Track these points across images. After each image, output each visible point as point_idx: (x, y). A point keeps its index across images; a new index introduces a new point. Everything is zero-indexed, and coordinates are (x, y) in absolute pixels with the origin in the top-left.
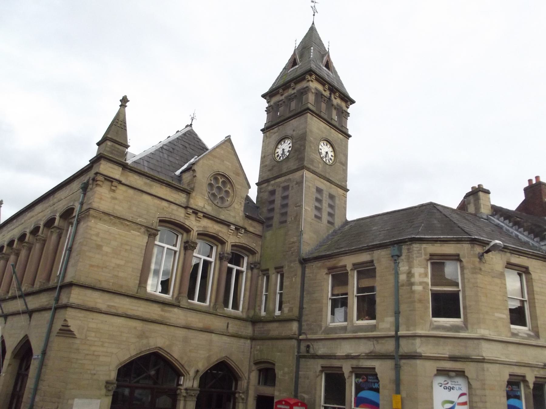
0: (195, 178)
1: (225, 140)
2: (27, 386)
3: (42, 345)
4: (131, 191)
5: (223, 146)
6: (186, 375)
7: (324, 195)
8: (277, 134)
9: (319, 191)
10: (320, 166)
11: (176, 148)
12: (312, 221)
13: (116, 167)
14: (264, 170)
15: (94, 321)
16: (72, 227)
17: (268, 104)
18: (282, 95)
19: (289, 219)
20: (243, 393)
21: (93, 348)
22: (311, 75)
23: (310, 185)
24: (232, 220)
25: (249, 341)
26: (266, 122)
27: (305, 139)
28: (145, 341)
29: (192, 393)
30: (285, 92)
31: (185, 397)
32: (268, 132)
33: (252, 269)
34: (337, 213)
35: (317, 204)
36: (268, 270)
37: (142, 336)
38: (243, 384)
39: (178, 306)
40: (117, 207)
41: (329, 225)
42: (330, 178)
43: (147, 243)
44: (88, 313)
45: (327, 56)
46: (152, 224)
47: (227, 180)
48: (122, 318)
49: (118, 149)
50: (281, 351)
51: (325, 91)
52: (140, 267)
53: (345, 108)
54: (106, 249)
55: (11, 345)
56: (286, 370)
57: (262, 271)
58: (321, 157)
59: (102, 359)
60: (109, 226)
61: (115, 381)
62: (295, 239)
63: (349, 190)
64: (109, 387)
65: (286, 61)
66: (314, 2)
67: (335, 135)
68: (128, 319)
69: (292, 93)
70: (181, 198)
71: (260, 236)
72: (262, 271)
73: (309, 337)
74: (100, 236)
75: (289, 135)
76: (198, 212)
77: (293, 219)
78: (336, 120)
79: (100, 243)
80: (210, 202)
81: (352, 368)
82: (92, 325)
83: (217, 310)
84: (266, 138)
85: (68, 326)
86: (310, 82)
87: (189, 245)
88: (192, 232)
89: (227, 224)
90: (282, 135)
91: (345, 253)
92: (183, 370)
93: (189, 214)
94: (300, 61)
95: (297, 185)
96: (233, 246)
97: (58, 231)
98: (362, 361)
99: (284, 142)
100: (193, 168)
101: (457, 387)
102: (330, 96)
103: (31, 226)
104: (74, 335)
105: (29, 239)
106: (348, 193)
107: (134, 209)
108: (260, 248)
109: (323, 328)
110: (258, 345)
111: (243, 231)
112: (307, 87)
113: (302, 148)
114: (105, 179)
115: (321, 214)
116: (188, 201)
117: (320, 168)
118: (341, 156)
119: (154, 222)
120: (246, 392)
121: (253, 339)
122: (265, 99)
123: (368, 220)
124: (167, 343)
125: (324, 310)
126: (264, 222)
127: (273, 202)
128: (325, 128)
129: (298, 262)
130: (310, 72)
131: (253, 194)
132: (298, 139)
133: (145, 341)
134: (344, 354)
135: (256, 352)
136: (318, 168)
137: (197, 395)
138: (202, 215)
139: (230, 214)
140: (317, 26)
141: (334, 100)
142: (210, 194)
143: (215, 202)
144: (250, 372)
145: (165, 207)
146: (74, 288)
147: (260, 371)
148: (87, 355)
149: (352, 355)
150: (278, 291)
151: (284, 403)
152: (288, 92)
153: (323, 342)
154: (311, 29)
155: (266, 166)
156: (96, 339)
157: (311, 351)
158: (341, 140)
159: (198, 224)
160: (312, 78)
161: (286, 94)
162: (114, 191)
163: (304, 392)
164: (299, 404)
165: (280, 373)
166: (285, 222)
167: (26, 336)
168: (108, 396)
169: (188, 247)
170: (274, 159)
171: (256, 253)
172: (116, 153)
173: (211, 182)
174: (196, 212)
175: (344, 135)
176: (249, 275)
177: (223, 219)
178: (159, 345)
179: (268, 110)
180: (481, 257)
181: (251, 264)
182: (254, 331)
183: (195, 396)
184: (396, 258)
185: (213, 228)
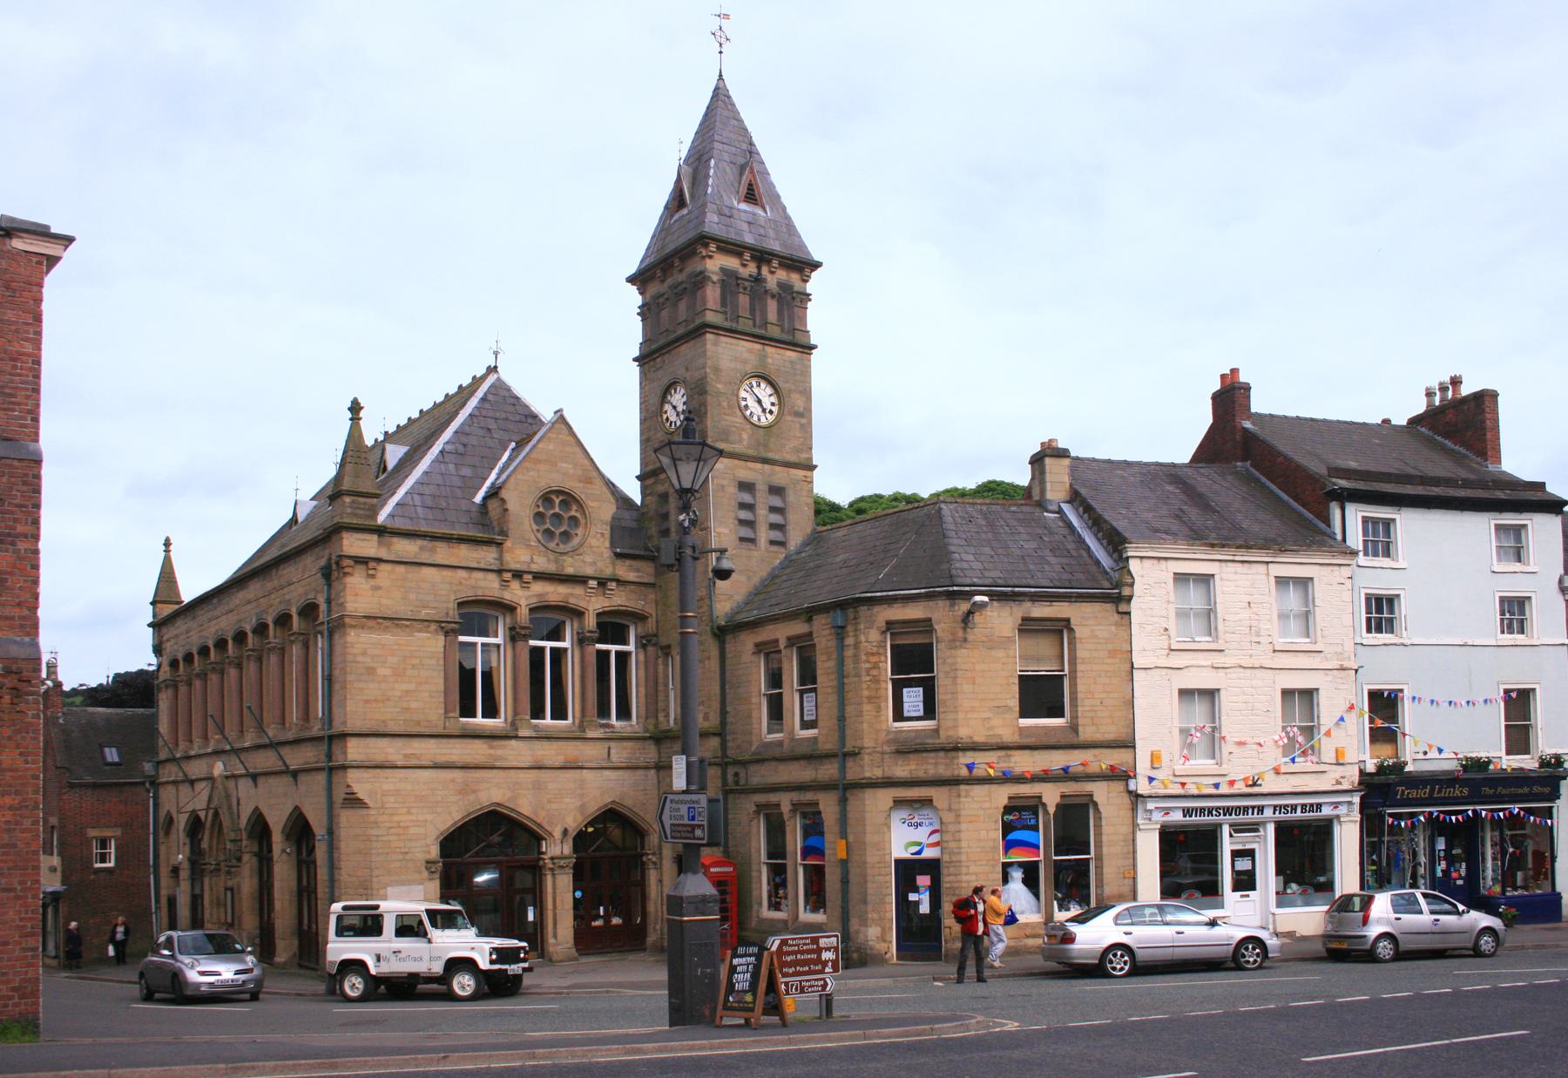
3: (325, 819)
4: (401, 569)
9: (746, 487)
10: (745, 436)
16: (322, 637)
20: (654, 854)
21: (396, 818)
27: (706, 392)
28: (472, 797)
29: (562, 862)
31: (552, 869)
33: (644, 646)
35: (744, 515)
36: (669, 647)
37: (463, 792)
39: (516, 737)
40: (384, 601)
43: (445, 646)
44: (378, 771)
46: (447, 614)
47: (568, 499)
51: (744, 266)
52: (442, 688)
53: (797, 285)
54: (382, 671)
55: (277, 821)
57: (662, 648)
58: (745, 417)
61: (438, 859)
67: (778, 357)
70: (487, 556)
71: (652, 585)
72: (662, 648)
79: (372, 665)
80: (544, 549)
81: (793, 805)
82: (385, 787)
87: (517, 633)
88: (518, 610)
89: (580, 580)
90: (665, 381)
96: (598, 615)
99: (675, 392)
101: (927, 821)
102: (759, 273)
104: (365, 804)
107: (412, 596)
108: (653, 605)
113: (703, 408)
116: (500, 559)
117: (743, 443)
124: (509, 794)
125: (755, 714)
128: (750, 351)
136: (741, 441)
137: (571, 865)
138: (530, 577)
139: (583, 561)
141: (769, 278)
146: (348, 739)
148: (390, 828)
159: (527, 593)
161: (669, 281)
162: (373, 576)
167: (297, 808)
171: (647, 618)
174: (518, 575)
176: (642, 657)
179: (645, 312)
180: (966, 619)
181: (643, 637)
184: (840, 632)
185: (556, 593)
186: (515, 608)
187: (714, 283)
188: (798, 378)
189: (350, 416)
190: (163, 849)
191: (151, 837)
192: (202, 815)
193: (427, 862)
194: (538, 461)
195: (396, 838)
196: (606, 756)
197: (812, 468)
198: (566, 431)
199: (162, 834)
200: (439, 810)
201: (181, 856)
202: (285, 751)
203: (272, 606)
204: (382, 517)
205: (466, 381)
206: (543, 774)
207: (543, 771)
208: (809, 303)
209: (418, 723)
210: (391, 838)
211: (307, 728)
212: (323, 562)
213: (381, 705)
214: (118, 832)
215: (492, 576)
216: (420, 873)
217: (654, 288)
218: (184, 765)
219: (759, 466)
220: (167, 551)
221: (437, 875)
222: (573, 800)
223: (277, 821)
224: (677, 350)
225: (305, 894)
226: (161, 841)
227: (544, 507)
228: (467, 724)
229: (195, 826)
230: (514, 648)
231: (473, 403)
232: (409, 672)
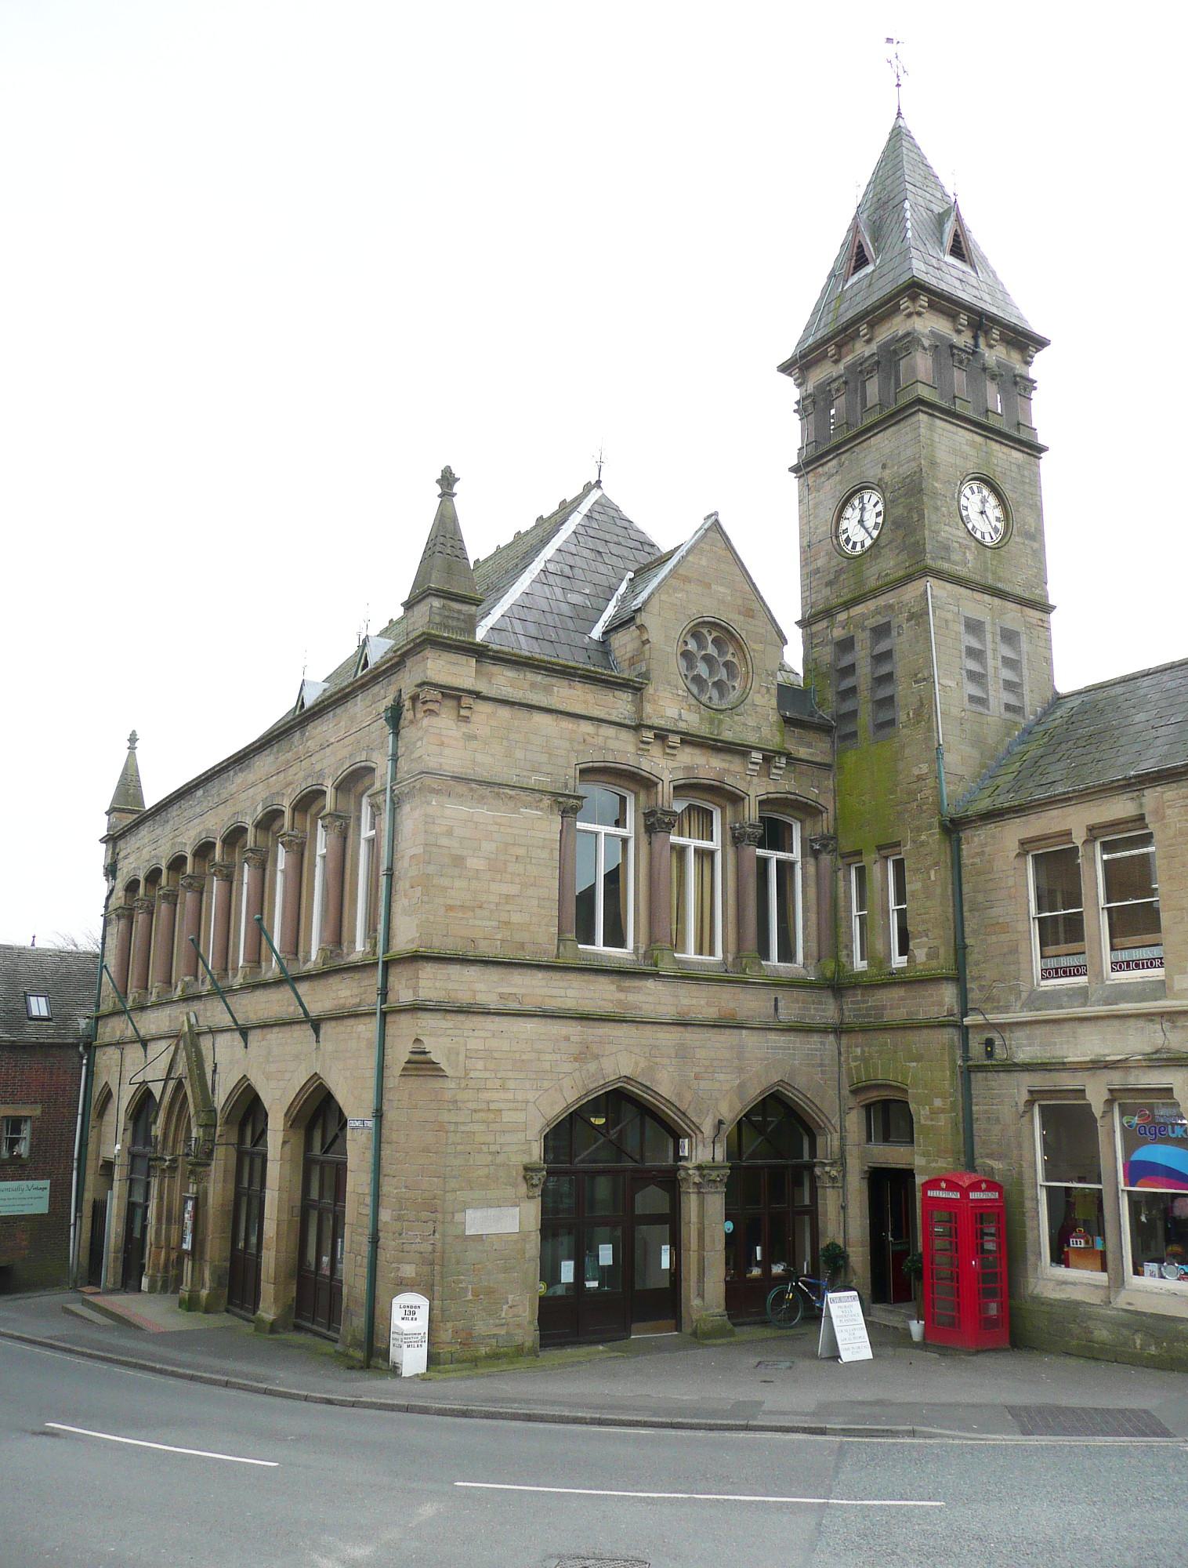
0: (647, 646)
1: (706, 527)
2: (348, 1189)
3: (370, 1096)
4: (504, 712)
5: (702, 545)
6: (692, 1134)
7: (989, 637)
8: (837, 478)
9: (974, 627)
11: (578, 562)
12: (963, 714)
13: (462, 659)
14: (814, 584)
15: (476, 1033)
19: (902, 717)
22: (914, 298)
23: (949, 616)
24: (752, 738)
25: (832, 1037)
26: (800, 446)
28: (592, 1067)
29: (714, 1175)
30: (844, 350)
31: (698, 1185)
32: (811, 474)
33: (816, 854)
35: (973, 665)
37: (584, 1055)
38: (829, 1143)
39: (655, 975)
40: (480, 758)
41: (1009, 715)
42: (1000, 585)
43: (561, 831)
44: (461, 1017)
45: (952, 218)
47: (725, 635)
48: (535, 1019)
49: (459, 612)
50: (918, 1058)
51: (959, 332)
53: (1019, 368)
54: (473, 863)
55: (278, 1099)
56: (938, 1103)
59: (507, 1117)
62: (924, 768)
64: (532, 1178)
65: (835, 250)
66: (895, 41)
67: (1005, 457)
68: (549, 1021)
69: (867, 354)
70: (620, 705)
71: (826, 767)
73: (994, 1018)
78: (999, 411)
80: (694, 702)
81: (1111, 1091)
82: (473, 1044)
83: (745, 970)
84: (806, 493)
85: (425, 1053)
86: (915, 317)
89: (738, 750)
91: (1064, 800)
92: (687, 1125)
93: (648, 743)
94: (878, 250)
95: (913, 622)
96: (761, 803)
97: (337, 824)
98: (1135, 1072)
100: (638, 621)
102: (976, 345)
103: (255, 809)
105: (255, 842)
106: (1052, 615)
108: (830, 796)
109: (1024, 995)
110: (857, 1048)
111: (784, 760)
112: (908, 334)
113: (915, 517)
115: (986, 691)
116: (639, 709)
117: (966, 563)
118: (1022, 515)
119: (566, 775)
120: (842, 1161)
121: (839, 1030)
122: (790, 375)
123: (1119, 690)
124: (642, 1065)
125: (1022, 948)
126: (832, 727)
127: (850, 670)
128: (972, 444)
129: (937, 830)
130: (914, 288)
131: (794, 656)
132: (899, 489)
134: (1088, 1059)
135: (853, 1064)
136: (965, 563)
138: (677, 739)
139: (745, 724)
140: (910, 123)
142: (690, 678)
143: (704, 699)
144: (843, 1113)
145: (588, 734)
147: (868, 1108)
149: (1108, 1059)
150: (892, 906)
151: (943, 1185)
153: (1027, 1030)
154: (895, 132)
155: (817, 571)
156: (487, 1075)
157: (1000, 1053)
158: (1019, 466)
159: (671, 764)
161: (848, 359)
162: (466, 719)
163: (990, 1156)
164: (984, 1186)
165: (922, 1112)
166: (891, 723)
168: (533, 1197)
169: (657, 826)
170: (839, 550)
173: (686, 648)
174: (661, 735)
175: (1026, 450)
176: (812, 870)
177: (730, 740)
178: (626, 1071)
183: (721, 1180)
185: (709, 766)
187: (924, 348)
188: (1027, 487)
189: (440, 491)
190: (92, 1135)
191: (79, 1117)
192: (156, 1089)
193: (526, 1169)
194: (687, 580)
195: (483, 1127)
196: (772, 1011)
197: (1047, 609)
199: (93, 1115)
200: (546, 1084)
201: (118, 1147)
202: (303, 988)
203: (291, 783)
204: (480, 635)
205: (549, 509)
206: (690, 1036)
207: (690, 1029)
209: (522, 946)
210: (476, 1127)
211: (338, 955)
212: (389, 701)
213: (470, 914)
214: (36, 1111)
215: (626, 736)
216: (515, 1185)
218: (137, 1017)
219: (987, 598)
220: (132, 748)
221: (538, 1192)
222: (728, 1077)
223: (278, 1099)
224: (865, 445)
225: (244, 1199)
226: (92, 1123)
228: (585, 952)
229: (144, 1104)
231: (575, 519)
232: (513, 867)
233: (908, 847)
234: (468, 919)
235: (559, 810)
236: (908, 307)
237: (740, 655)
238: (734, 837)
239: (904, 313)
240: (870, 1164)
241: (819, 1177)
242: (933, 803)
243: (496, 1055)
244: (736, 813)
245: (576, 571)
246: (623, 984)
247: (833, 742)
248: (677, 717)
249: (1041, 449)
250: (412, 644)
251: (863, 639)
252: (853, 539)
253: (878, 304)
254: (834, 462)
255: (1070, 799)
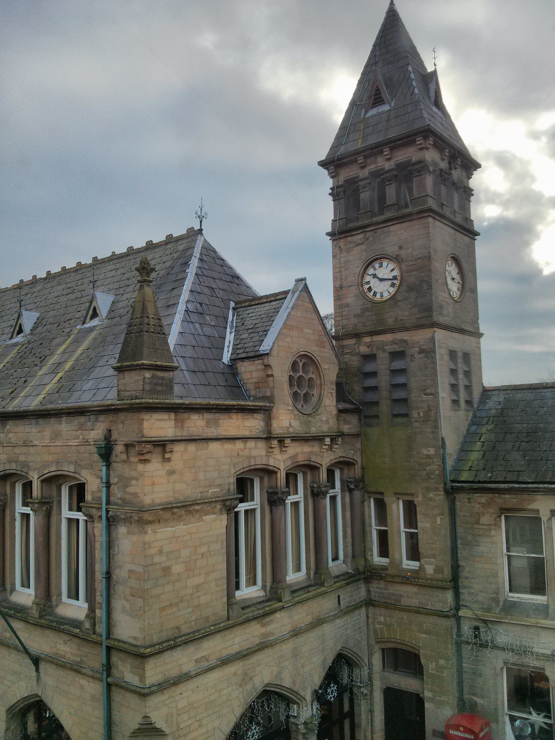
8: (363, 247)
9: (452, 354)
13: (165, 416)
17: (331, 180)
18: (363, 168)
19: (414, 414)
22: (425, 138)
28: (249, 687)
30: (369, 161)
31: (304, 734)
32: (342, 240)
33: (351, 491)
34: (474, 379)
48: (217, 670)
49: (163, 378)
51: (443, 160)
54: (177, 569)
60: (173, 527)
62: (432, 451)
63: (483, 334)
74: (164, 551)
75: (391, 254)
76: (283, 439)
77: (421, 414)
79: (167, 564)
84: (338, 252)
85: (151, 724)
89: (319, 439)
95: (422, 355)
97: (44, 508)
99: (381, 266)
104: (162, 731)
108: (358, 454)
109: (501, 604)
112: (420, 162)
114: (154, 445)
122: (327, 169)
133: (249, 687)
139: (321, 421)
145: (240, 449)
152: (375, 162)
159: (285, 457)
160: (429, 144)
162: (169, 460)
165: (430, 666)
171: (354, 464)
172: (160, 388)
176: (348, 500)
178: (266, 681)
182: (369, 591)
186: (276, 473)
198: (307, 299)
208: (472, 197)
217: (346, 174)
224: (386, 229)
227: (293, 372)
230: (271, 511)
233: (420, 499)
234: (174, 613)
235: (226, 510)
236: (421, 144)
237: (316, 372)
238: (312, 492)
239: (419, 147)
240: (387, 685)
241: (355, 694)
242: (438, 475)
243: (195, 705)
244: (313, 476)
245: (204, 306)
246: (264, 621)
247: (360, 420)
248: (288, 426)
249: (477, 234)
250: (128, 406)
251: (383, 357)
252: (374, 289)
253: (400, 137)
254: (361, 236)
255: (539, 491)
